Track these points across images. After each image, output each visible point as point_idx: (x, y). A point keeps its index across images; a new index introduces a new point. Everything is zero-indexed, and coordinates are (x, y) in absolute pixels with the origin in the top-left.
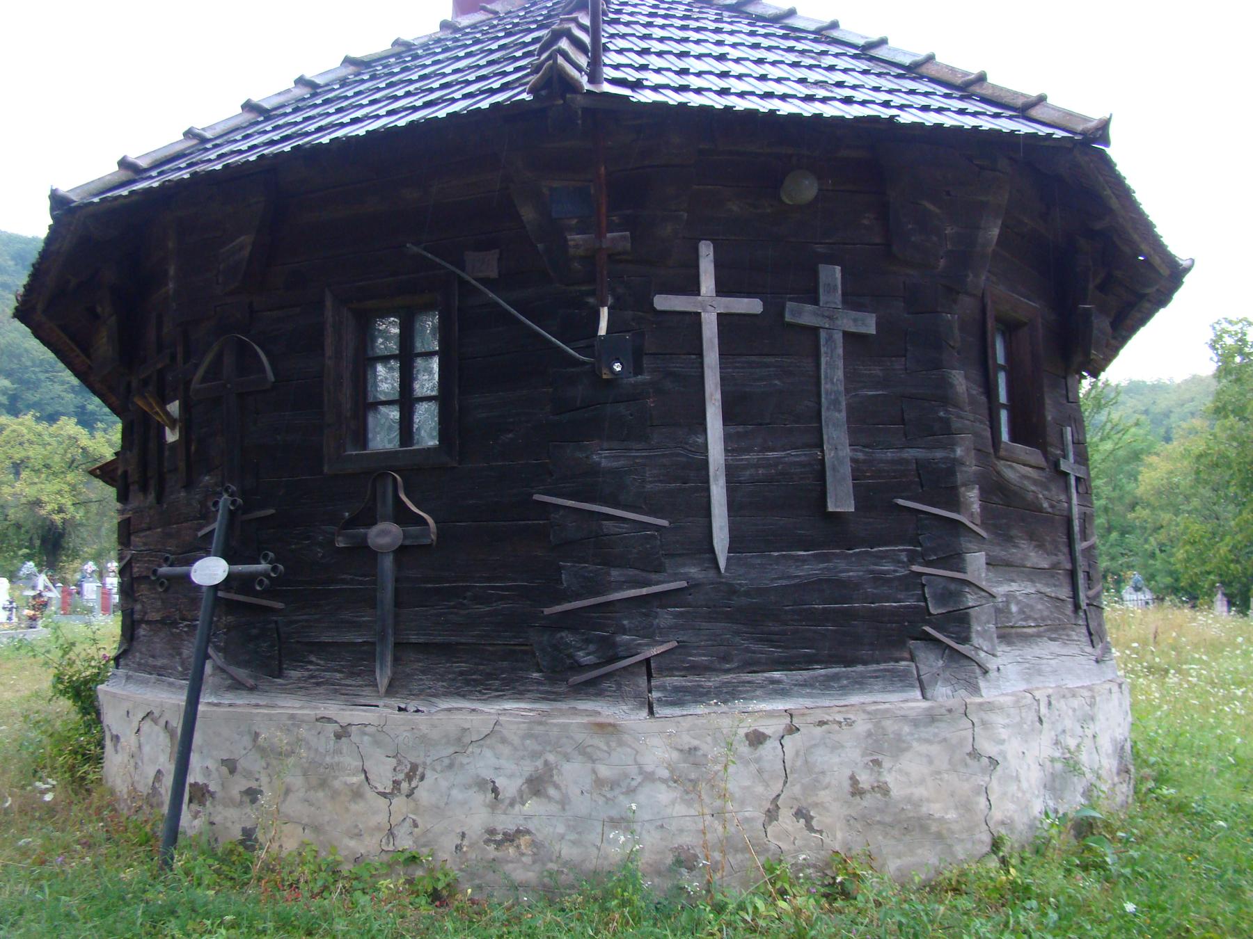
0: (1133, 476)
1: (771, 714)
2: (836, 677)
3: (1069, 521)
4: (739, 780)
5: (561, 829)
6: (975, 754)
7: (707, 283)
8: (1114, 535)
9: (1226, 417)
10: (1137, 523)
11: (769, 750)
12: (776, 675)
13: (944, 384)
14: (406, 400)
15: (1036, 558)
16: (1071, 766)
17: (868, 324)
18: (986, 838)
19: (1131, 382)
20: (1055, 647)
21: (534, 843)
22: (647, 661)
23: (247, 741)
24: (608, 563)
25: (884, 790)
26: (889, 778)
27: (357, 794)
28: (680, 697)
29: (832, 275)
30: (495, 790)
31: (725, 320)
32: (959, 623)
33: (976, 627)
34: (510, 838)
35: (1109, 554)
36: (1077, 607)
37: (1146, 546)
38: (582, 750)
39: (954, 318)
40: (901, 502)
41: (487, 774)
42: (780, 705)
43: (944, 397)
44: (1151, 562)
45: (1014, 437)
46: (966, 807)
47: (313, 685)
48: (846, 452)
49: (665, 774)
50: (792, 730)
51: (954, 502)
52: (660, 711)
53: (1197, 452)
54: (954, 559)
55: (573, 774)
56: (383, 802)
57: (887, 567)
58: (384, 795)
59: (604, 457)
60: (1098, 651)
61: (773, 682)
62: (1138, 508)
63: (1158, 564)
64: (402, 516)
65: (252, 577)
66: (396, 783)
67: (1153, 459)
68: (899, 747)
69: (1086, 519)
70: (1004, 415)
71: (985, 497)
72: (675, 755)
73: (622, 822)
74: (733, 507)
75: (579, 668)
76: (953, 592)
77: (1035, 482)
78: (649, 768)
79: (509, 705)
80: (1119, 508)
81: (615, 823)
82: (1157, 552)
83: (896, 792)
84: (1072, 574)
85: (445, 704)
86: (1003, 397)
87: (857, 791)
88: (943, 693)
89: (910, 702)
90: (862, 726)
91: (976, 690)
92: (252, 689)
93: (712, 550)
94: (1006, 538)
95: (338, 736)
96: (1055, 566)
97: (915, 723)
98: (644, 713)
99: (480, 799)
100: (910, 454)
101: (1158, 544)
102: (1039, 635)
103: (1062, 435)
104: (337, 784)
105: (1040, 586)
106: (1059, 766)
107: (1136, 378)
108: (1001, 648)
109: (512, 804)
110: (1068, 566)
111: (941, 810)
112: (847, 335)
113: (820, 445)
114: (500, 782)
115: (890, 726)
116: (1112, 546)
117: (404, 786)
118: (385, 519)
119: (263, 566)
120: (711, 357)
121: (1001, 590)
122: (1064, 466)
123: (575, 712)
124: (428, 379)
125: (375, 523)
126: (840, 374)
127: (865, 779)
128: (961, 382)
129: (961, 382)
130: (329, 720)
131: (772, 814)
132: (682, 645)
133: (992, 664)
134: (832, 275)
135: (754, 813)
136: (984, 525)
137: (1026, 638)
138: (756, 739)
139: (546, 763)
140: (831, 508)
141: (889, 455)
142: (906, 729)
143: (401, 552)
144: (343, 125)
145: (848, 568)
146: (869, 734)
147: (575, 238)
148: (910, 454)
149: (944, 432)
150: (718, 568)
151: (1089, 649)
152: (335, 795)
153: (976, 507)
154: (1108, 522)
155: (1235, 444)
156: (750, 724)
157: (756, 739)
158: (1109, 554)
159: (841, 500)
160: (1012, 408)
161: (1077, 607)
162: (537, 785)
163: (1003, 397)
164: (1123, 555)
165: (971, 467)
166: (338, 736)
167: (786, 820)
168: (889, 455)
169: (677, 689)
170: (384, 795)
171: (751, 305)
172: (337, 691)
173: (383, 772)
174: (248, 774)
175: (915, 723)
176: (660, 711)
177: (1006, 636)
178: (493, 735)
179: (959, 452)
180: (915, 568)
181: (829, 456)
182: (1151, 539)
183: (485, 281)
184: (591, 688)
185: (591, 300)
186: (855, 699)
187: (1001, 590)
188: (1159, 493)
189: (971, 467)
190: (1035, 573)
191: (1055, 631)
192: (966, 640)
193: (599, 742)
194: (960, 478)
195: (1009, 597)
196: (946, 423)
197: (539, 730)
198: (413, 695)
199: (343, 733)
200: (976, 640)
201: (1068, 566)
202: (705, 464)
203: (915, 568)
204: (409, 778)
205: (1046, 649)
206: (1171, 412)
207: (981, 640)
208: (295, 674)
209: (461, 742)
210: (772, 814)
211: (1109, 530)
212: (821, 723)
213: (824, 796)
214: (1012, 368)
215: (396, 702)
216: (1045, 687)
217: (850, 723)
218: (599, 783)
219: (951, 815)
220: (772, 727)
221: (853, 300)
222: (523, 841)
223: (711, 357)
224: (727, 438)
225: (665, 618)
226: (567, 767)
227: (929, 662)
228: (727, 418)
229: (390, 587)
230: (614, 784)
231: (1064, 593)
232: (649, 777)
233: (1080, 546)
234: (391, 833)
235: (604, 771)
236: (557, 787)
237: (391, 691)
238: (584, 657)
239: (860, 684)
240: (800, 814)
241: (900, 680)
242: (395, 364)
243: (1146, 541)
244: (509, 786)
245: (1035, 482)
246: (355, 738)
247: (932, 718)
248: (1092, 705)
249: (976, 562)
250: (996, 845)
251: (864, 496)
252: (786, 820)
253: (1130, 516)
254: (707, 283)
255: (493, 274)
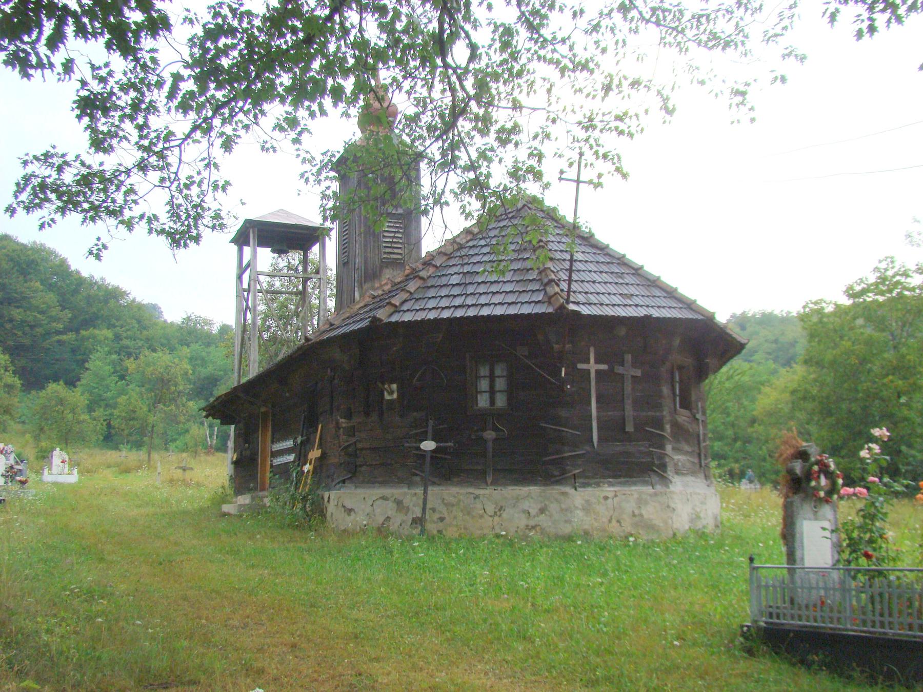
0: (753, 400)
1: (610, 491)
2: (628, 481)
3: (698, 436)
4: (600, 509)
5: (550, 524)
6: (668, 507)
7: (592, 360)
8: (738, 444)
9: (811, 366)
10: (754, 435)
11: (610, 501)
12: (611, 480)
13: (661, 391)
14: (492, 392)
15: (687, 448)
16: (698, 517)
17: (638, 373)
18: (671, 533)
19: (763, 315)
20: (693, 478)
21: (541, 529)
22: (574, 475)
23: (439, 501)
24: (563, 444)
25: (641, 515)
26: (644, 512)
27: (481, 517)
28: (585, 485)
29: (628, 357)
30: (529, 513)
31: (597, 372)
32: (663, 467)
33: (669, 469)
34: (533, 527)
35: (734, 458)
36: (701, 466)
37: (760, 452)
38: (556, 500)
39: (663, 370)
40: (647, 429)
41: (526, 508)
42: (612, 489)
43: (661, 396)
44: (763, 464)
45: (681, 407)
46: (666, 523)
47: (461, 483)
48: (631, 413)
49: (581, 507)
50: (616, 496)
51: (663, 429)
52: (579, 489)
53: (791, 389)
54: (662, 447)
55: (553, 507)
56: (491, 519)
57: (642, 448)
58: (491, 516)
59: (563, 413)
60: (708, 482)
61: (610, 482)
62: (756, 425)
63: (768, 466)
64: (496, 429)
65: (446, 448)
66: (495, 513)
67: (766, 390)
68: (646, 503)
69: (705, 435)
70: (678, 398)
71: (672, 426)
72: (583, 502)
73: (568, 521)
74: (599, 429)
75: (555, 476)
76: (662, 457)
77: (687, 422)
78: (577, 505)
79: (531, 488)
80: (743, 424)
81: (566, 521)
82: (767, 457)
83: (646, 516)
84: (699, 455)
85: (510, 488)
86: (677, 392)
87: (634, 515)
88: (659, 488)
89: (649, 489)
90: (636, 496)
91: (668, 487)
92: (439, 485)
93: (592, 442)
94: (678, 441)
95: (475, 498)
96: (694, 451)
97: (651, 495)
98: (573, 490)
99: (523, 516)
100: (650, 413)
101: (768, 451)
102: (688, 474)
103: (697, 406)
104: (474, 514)
105: (688, 458)
106: (694, 516)
107: (768, 310)
108: (676, 476)
109: (534, 516)
110: (698, 451)
111: (658, 522)
112: (633, 377)
113: (624, 411)
114: (531, 511)
115: (644, 497)
116: (737, 452)
117: (498, 513)
118: (490, 429)
119: (450, 444)
120: (593, 383)
121: (676, 457)
122: (698, 416)
123: (553, 489)
124: (500, 384)
125: (486, 430)
126: (630, 389)
127: (637, 512)
128: (666, 390)
129: (666, 390)
130: (472, 493)
131: (610, 521)
132: (584, 470)
133: (673, 480)
134: (628, 357)
135: (605, 520)
136: (671, 437)
137: (683, 474)
138: (606, 498)
139: (545, 504)
140: (627, 430)
141: (644, 414)
142: (648, 498)
143: (496, 440)
144: (394, 253)
145: (630, 448)
146: (638, 498)
147: (556, 346)
148: (650, 413)
149: (658, 407)
150: (593, 445)
151: (705, 481)
152: (473, 517)
153: (669, 431)
154: (735, 434)
155: (817, 384)
156: (604, 494)
157: (606, 498)
158: (734, 458)
159: (630, 428)
160: (680, 396)
161: (701, 466)
162: (542, 511)
163: (677, 392)
164: (744, 458)
165: (668, 418)
166: (475, 498)
167: (614, 523)
168: (644, 414)
169: (583, 483)
170: (491, 516)
171: (604, 367)
172: (472, 485)
173: (490, 509)
174: (440, 512)
175: (651, 495)
176: (579, 489)
177: (677, 472)
178: (529, 496)
179: (665, 413)
180: (651, 449)
181: (626, 414)
182: (764, 447)
183: (525, 356)
184: (558, 482)
185: (558, 365)
186: (633, 488)
187: (676, 457)
188: (770, 414)
189: (668, 418)
190: (686, 453)
191: (693, 473)
192: (665, 472)
193: (562, 498)
194: (665, 421)
195: (679, 460)
196: (661, 404)
197: (543, 494)
198: (500, 485)
199: (477, 497)
200: (669, 473)
201: (698, 451)
202: (591, 416)
203: (651, 449)
204: (500, 510)
205: (690, 479)
206: (796, 342)
207: (670, 473)
208: (455, 480)
209: (518, 499)
210: (610, 521)
211: (735, 440)
212: (624, 494)
213: (625, 516)
214: (681, 382)
215: (493, 487)
216: (690, 490)
217: (632, 495)
218: (562, 510)
219: (661, 525)
220: (610, 495)
221: (634, 365)
222: (538, 528)
223: (593, 383)
224: (598, 408)
225: (579, 462)
226: (552, 505)
227: (655, 479)
228: (598, 402)
229: (491, 450)
230: (567, 510)
231: (696, 461)
232: (577, 508)
233: (703, 444)
234: (493, 528)
235: (563, 506)
236: (549, 511)
237: (492, 484)
238: (556, 473)
239: (635, 484)
240: (618, 521)
241: (646, 483)
242: (488, 379)
243: (761, 449)
244: (533, 512)
245: (687, 422)
246: (481, 498)
247: (656, 494)
248: (705, 499)
249: (669, 448)
250: (674, 534)
251: (636, 426)
252: (614, 523)
253: (750, 430)
254: (592, 360)
255: (527, 353)
